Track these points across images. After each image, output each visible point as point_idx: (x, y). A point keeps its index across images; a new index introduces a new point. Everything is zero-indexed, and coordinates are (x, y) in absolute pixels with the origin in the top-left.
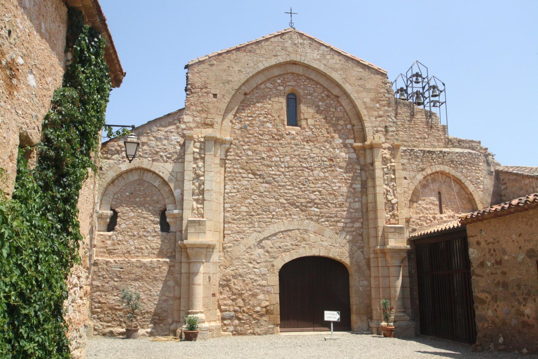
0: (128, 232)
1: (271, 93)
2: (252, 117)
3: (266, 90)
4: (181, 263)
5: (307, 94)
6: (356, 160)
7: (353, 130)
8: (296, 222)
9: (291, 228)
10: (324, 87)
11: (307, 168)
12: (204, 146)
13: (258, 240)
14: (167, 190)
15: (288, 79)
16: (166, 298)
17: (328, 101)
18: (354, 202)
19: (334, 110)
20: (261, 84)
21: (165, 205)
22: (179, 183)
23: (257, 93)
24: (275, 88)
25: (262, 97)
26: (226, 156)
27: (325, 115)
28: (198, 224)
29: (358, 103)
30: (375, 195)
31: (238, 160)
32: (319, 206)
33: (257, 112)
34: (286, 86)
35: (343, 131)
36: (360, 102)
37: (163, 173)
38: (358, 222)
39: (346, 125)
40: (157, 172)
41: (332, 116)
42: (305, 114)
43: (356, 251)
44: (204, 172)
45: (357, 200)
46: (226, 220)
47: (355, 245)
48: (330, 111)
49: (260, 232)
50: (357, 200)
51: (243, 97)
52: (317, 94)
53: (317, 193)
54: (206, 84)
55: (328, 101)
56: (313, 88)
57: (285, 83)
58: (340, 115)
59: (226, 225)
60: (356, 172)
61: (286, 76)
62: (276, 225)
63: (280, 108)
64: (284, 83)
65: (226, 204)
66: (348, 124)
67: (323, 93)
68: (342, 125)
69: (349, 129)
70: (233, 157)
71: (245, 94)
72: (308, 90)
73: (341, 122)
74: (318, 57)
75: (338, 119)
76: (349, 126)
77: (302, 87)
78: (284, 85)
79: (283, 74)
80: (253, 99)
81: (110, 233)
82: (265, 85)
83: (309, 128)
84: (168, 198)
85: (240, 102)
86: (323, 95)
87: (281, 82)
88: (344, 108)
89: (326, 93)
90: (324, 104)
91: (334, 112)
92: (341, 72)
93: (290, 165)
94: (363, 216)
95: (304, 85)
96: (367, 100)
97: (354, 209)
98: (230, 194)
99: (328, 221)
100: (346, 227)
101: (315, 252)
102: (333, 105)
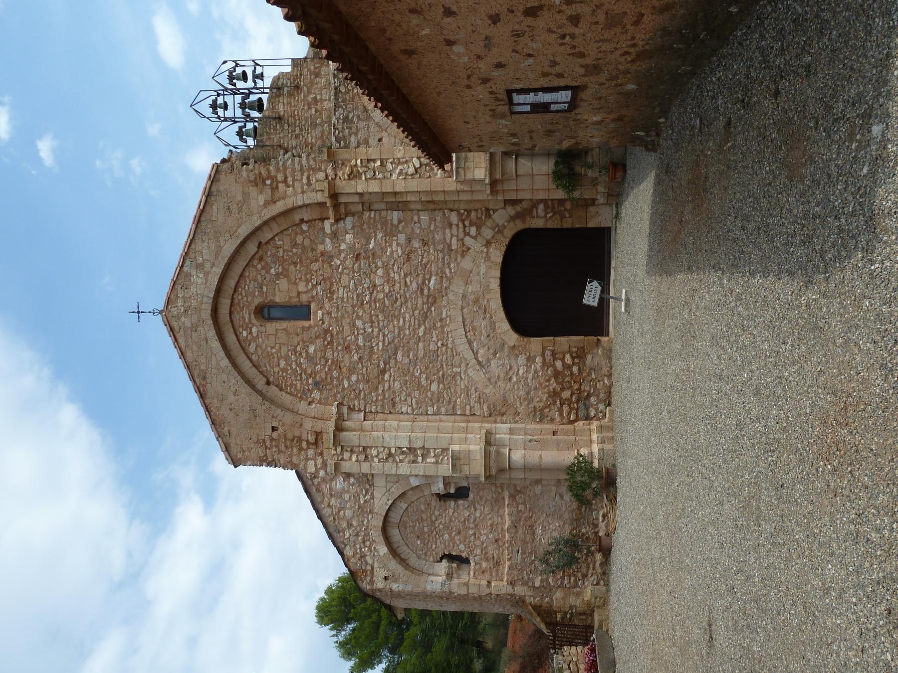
0: (470, 542)
2: (301, 375)
5: (261, 292)
8: (452, 312)
11: (371, 294)
13: (478, 367)
18: (419, 222)
26: (360, 410)
27: (290, 265)
28: (457, 461)
29: (268, 213)
32: (427, 277)
36: (265, 211)
38: (449, 218)
39: (303, 232)
42: (291, 295)
45: (416, 218)
46: (451, 412)
48: (283, 257)
49: (468, 364)
50: (416, 218)
53: (408, 280)
54: (258, 441)
60: (375, 218)
61: (236, 324)
62: (457, 342)
64: (247, 326)
67: (256, 267)
68: (304, 238)
69: (309, 227)
71: (268, 383)
73: (299, 239)
81: (472, 564)
83: (312, 289)
86: (259, 266)
87: (246, 330)
88: (277, 235)
89: (255, 262)
90: (273, 265)
91: (284, 251)
92: (222, 240)
96: (261, 199)
99: (449, 264)
100: (457, 236)
101: (495, 284)
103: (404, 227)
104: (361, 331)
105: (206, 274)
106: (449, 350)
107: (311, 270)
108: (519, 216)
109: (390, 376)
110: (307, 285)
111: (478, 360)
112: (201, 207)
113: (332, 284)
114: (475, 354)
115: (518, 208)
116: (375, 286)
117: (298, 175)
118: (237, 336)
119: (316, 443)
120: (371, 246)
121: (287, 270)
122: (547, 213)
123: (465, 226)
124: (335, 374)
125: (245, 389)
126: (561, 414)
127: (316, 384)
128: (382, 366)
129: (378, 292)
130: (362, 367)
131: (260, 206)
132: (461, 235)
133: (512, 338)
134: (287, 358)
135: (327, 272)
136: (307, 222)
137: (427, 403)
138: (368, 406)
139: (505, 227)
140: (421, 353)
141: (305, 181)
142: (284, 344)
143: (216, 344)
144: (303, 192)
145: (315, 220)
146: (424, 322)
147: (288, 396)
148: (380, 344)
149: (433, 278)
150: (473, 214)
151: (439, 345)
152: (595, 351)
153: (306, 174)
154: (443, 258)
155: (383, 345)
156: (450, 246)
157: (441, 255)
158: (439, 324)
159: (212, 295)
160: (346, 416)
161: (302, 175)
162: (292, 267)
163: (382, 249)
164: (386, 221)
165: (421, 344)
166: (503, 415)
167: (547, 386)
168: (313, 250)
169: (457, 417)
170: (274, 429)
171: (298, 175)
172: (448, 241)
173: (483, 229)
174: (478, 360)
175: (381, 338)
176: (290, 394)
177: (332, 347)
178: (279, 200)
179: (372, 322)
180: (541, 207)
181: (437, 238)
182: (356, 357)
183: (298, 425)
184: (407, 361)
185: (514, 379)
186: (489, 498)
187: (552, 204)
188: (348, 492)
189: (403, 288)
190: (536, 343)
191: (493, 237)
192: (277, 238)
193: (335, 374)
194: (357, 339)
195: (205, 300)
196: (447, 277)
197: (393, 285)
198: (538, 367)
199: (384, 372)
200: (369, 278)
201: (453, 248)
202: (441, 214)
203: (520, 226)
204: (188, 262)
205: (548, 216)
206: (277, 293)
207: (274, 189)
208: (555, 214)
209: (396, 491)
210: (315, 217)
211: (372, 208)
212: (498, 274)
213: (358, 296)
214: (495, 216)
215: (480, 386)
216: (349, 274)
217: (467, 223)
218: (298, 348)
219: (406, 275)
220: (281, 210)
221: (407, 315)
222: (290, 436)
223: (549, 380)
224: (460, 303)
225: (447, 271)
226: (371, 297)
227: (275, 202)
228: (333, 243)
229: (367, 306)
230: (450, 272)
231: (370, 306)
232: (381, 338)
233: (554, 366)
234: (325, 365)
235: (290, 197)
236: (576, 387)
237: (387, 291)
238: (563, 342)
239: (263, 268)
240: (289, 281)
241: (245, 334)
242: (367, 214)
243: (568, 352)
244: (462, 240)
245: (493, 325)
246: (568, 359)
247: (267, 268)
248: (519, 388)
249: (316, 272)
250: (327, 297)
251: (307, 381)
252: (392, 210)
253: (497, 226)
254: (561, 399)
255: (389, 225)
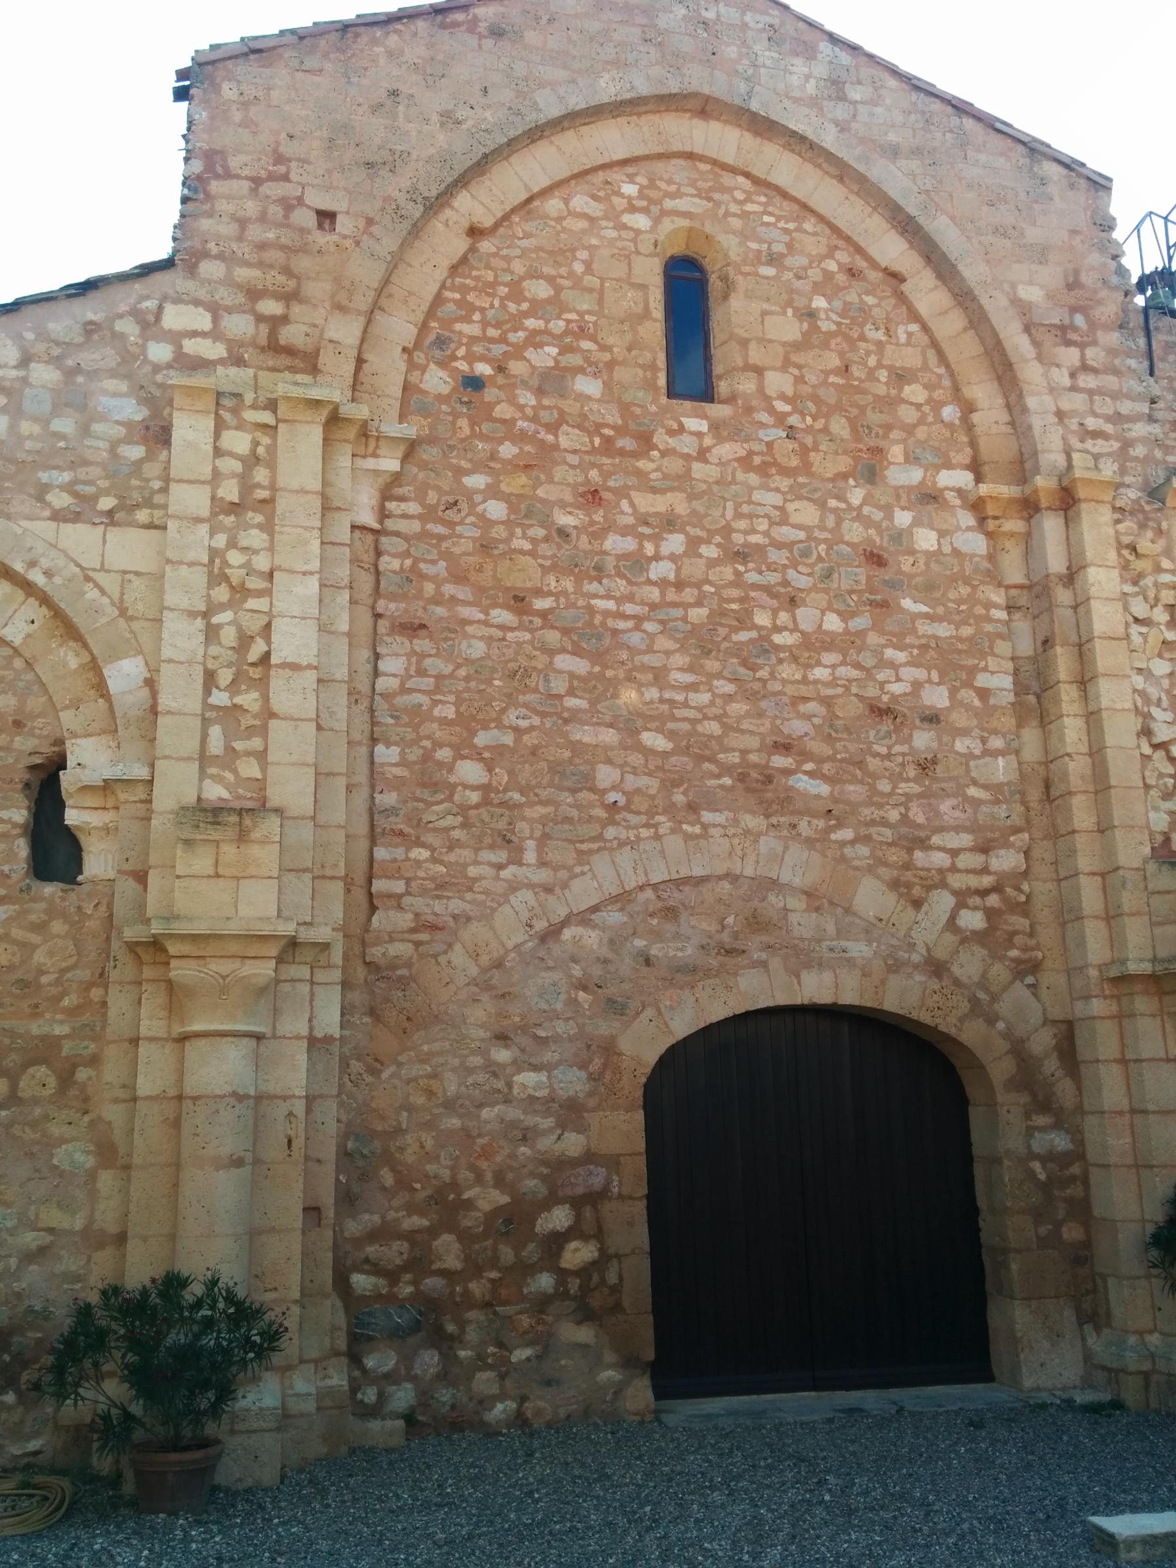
1: (594, 241)
2: (503, 340)
3: (569, 223)
4: (135, 1041)
5: (758, 259)
6: (986, 564)
7: (970, 428)
8: (719, 843)
9: (698, 872)
10: (835, 230)
11: (767, 589)
12: (272, 449)
13: (540, 925)
14: (73, 663)
15: (670, 182)
16: (48, 1238)
17: (852, 297)
18: (987, 753)
19: (880, 335)
20: (545, 192)
21: (60, 742)
22: (136, 625)
23: (527, 236)
24: (613, 215)
25: (551, 253)
26: (383, 515)
27: (841, 354)
28: (231, 833)
29: (996, 306)
30: (1093, 718)
31: (441, 538)
32: (826, 768)
33: (531, 323)
34: (664, 213)
35: (921, 433)
36: (1004, 302)
37: (48, 574)
38: (1007, 845)
39: (937, 406)
40: (19, 567)
41: (872, 361)
42: (753, 346)
43: (1005, 989)
44: (271, 575)
45: (997, 743)
46: (381, 822)
47: (1002, 958)
48: (863, 338)
49: (549, 890)
50: (997, 743)
51: (461, 245)
52: (804, 261)
53: (812, 707)
54: (280, 159)
55: (852, 297)
56: (786, 231)
57: (659, 202)
58: (910, 358)
59: (381, 853)
60: (989, 620)
61: (659, 167)
62: (625, 857)
63: (639, 309)
64: (651, 201)
65: (380, 749)
66: (944, 404)
67: (830, 255)
68: (918, 406)
69: (950, 426)
70: (416, 526)
71: (474, 232)
72: (760, 241)
73: (915, 392)
74: (811, 88)
75: (901, 377)
76: (950, 412)
77: (736, 223)
78: (655, 210)
79: (648, 158)
80: (508, 259)
82: (566, 202)
83: (771, 410)
84: (76, 704)
85: (446, 263)
86: (832, 266)
87: (641, 195)
88: (925, 328)
89: (843, 257)
90: (838, 304)
91: (880, 344)
92: (914, 165)
93: (685, 572)
94: (1028, 821)
95: (745, 215)
96: (1032, 294)
97: (985, 787)
98: (400, 700)
99: (867, 839)
100: (954, 869)
101: (815, 988)
102: (876, 312)
103: (968, 707)
104: (649, 549)
105: (814, 102)
106: (595, 829)
107: (827, 416)
108: (1027, 1075)
109: (502, 627)
110: (783, 397)
111: (565, 923)
112: (998, 125)
113: (785, 472)
114: (584, 918)
115: (1051, 1066)
116: (793, 602)
117: (1106, 406)
118: (625, 162)
119: (274, 347)
120: (907, 603)
121: (825, 345)
122: (1045, 1159)
123: (984, 893)
124: (507, 450)
125: (461, 148)
126: (373, 1236)
127: (474, 383)
128: (541, 604)
129: (775, 613)
130: (533, 541)
131: (1013, 286)
132: (957, 881)
133: (645, 1044)
134: (557, 304)
135: (827, 464)
136: (965, 418)
137: (416, 742)
138: (400, 545)
139: (991, 1020)
140: (584, 734)
141: (1091, 423)
142: (600, 301)
143: (608, 88)
144: (1060, 415)
145: (973, 444)
146: (686, 751)
147: (433, 288)
148: (611, 605)
149: (824, 789)
150: (1019, 922)
151: (612, 797)
152: (610, 1357)
153: (1109, 428)
154: (884, 823)
155: (607, 613)
156: (923, 844)
157: (894, 815)
158: (679, 798)
159: (754, 106)
160: (370, 463)
161: (1108, 419)
162: (834, 361)
163: (901, 635)
164: (983, 655)
165: (609, 736)
166: (372, 1012)
167: (479, 1179)
168: (888, 428)
169: (363, 845)
170: (326, 217)
171: (1106, 406)
172: (936, 840)
173: (980, 952)
174: (565, 923)
175: (629, 609)
176: (438, 300)
177: (593, 451)
178: (1036, 343)
179: (679, 585)
180: (1061, 1142)
181: (945, 806)
182: (565, 520)
183: (342, 297)
184: (559, 685)
185: (502, 1055)
186: (39, 957)
187: (1073, 1179)
188: (85, 430)
189: (790, 690)
190: (623, 1129)
191: (957, 983)
192: (914, 327)
193: (507, 450)
194: (625, 531)
195: (743, 87)
196: (829, 830)
197: (795, 659)
198: (545, 1143)
199: (519, 601)
200: (814, 588)
201: (918, 855)
202: (1017, 820)
203: (1000, 1070)
204: (845, 58)
205: (1036, 1166)
206: (757, 307)
207: (1064, 335)
208: (1046, 1188)
209: (92, 608)
210: (983, 443)
211: (1017, 616)
212: (848, 998)
213: (760, 549)
214: (1020, 991)
215: (475, 931)
216: (822, 528)
217: (993, 900)
218: (586, 345)
219: (827, 702)
220: (1007, 345)
221: (704, 698)
222: (303, 264)
223: (500, 1181)
224: (749, 871)
225: (847, 834)
226: (755, 587)
227: (1027, 329)
228: (910, 489)
229: (728, 573)
230: (843, 844)
231: (732, 584)
232: (629, 609)
233: (551, 1200)
234: (534, 419)
235: (1045, 375)
236: (477, 1288)
237: (778, 639)
238: (631, 1230)
239: (828, 275)
240: (797, 347)
241: (630, 189)
242: (998, 597)
243: (602, 1251)
244: (943, 884)
245: (686, 974)
246: (578, 1254)
247: (825, 286)
248: (471, 1071)
249: (825, 430)
250: (751, 453)
251: (483, 359)
252: (1016, 673)
253: (994, 998)
254: (433, 1232)
255: (970, 662)
